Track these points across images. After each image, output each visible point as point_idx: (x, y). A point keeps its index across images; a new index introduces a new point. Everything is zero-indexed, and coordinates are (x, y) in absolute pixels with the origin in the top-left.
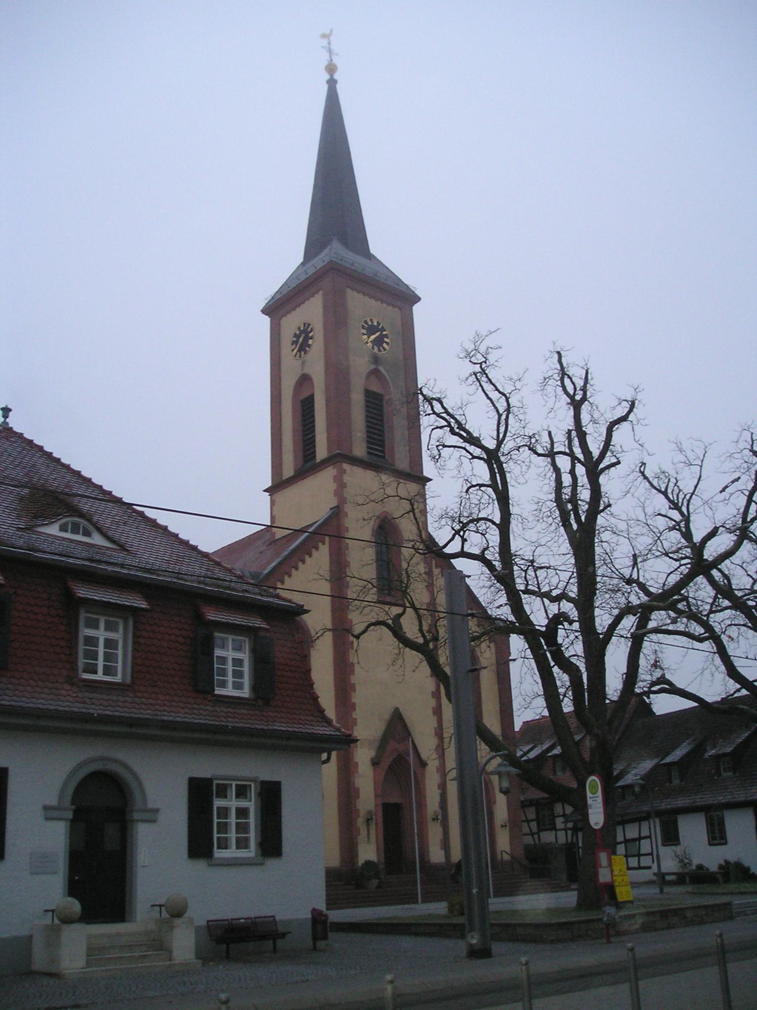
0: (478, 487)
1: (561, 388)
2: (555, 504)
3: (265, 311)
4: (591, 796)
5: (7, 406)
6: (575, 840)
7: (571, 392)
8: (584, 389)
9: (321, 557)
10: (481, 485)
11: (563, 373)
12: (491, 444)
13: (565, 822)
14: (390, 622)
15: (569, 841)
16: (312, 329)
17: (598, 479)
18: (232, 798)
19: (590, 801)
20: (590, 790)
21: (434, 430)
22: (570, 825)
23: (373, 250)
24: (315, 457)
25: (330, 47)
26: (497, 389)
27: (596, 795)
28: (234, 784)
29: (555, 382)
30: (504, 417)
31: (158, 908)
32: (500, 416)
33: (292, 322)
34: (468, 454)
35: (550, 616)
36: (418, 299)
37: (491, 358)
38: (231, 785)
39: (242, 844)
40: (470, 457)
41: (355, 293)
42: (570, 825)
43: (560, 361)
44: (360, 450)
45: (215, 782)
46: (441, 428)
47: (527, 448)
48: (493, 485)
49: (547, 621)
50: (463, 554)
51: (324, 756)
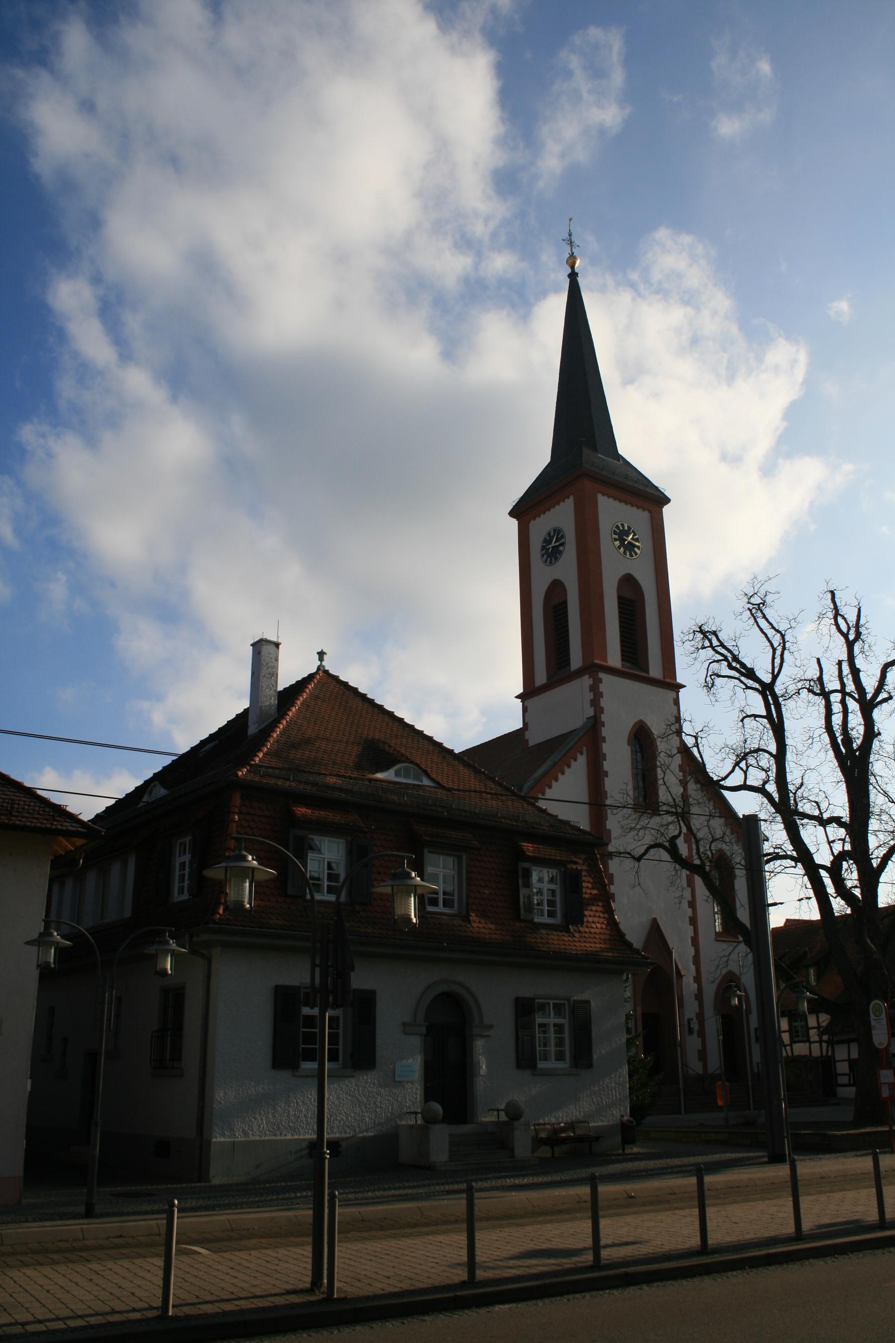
0: (753, 718)
1: (835, 627)
2: (825, 730)
3: (512, 513)
4: (875, 1018)
5: (322, 650)
6: (830, 1053)
7: (845, 630)
8: (857, 625)
9: (579, 766)
10: (755, 716)
11: (837, 613)
12: (767, 678)
13: (820, 1035)
14: (667, 844)
15: (824, 1054)
16: (562, 535)
17: (872, 712)
18: (550, 1014)
19: (873, 1023)
20: (873, 1012)
21: (712, 664)
22: (825, 1037)
23: (621, 451)
24: (569, 664)
25: (571, 239)
26: (773, 627)
27: (880, 1018)
28: (551, 1002)
29: (829, 621)
30: (778, 652)
31: (495, 1113)
32: (774, 650)
33: (541, 527)
34: (741, 684)
35: (836, 853)
36: (667, 500)
37: (768, 599)
38: (549, 1004)
39: (560, 1057)
40: (745, 687)
41: (605, 498)
42: (825, 1037)
43: (833, 600)
44: (614, 658)
45: (537, 1001)
46: (718, 661)
47: (806, 690)
48: (769, 717)
49: (832, 858)
50: (745, 787)
51: (624, 977)
